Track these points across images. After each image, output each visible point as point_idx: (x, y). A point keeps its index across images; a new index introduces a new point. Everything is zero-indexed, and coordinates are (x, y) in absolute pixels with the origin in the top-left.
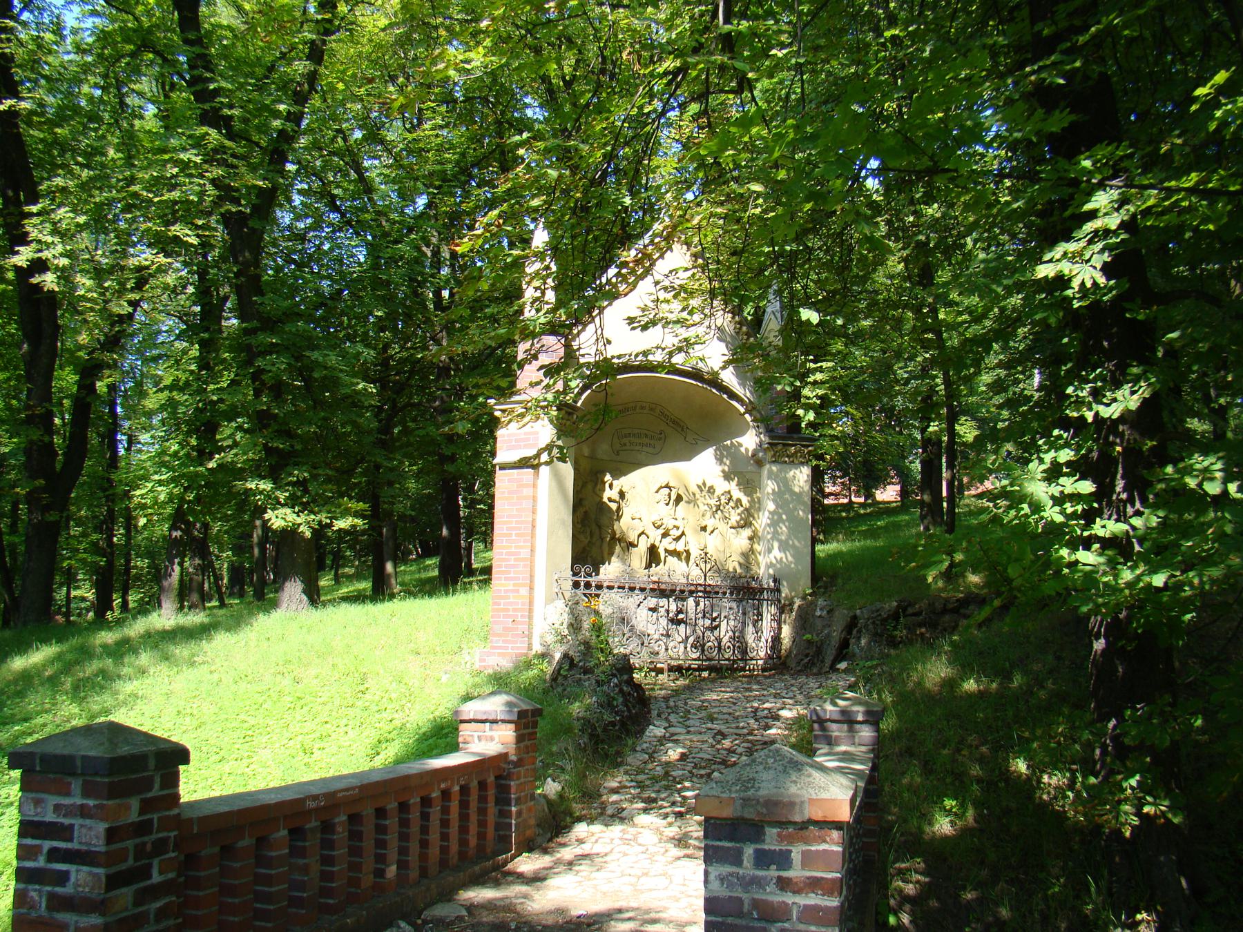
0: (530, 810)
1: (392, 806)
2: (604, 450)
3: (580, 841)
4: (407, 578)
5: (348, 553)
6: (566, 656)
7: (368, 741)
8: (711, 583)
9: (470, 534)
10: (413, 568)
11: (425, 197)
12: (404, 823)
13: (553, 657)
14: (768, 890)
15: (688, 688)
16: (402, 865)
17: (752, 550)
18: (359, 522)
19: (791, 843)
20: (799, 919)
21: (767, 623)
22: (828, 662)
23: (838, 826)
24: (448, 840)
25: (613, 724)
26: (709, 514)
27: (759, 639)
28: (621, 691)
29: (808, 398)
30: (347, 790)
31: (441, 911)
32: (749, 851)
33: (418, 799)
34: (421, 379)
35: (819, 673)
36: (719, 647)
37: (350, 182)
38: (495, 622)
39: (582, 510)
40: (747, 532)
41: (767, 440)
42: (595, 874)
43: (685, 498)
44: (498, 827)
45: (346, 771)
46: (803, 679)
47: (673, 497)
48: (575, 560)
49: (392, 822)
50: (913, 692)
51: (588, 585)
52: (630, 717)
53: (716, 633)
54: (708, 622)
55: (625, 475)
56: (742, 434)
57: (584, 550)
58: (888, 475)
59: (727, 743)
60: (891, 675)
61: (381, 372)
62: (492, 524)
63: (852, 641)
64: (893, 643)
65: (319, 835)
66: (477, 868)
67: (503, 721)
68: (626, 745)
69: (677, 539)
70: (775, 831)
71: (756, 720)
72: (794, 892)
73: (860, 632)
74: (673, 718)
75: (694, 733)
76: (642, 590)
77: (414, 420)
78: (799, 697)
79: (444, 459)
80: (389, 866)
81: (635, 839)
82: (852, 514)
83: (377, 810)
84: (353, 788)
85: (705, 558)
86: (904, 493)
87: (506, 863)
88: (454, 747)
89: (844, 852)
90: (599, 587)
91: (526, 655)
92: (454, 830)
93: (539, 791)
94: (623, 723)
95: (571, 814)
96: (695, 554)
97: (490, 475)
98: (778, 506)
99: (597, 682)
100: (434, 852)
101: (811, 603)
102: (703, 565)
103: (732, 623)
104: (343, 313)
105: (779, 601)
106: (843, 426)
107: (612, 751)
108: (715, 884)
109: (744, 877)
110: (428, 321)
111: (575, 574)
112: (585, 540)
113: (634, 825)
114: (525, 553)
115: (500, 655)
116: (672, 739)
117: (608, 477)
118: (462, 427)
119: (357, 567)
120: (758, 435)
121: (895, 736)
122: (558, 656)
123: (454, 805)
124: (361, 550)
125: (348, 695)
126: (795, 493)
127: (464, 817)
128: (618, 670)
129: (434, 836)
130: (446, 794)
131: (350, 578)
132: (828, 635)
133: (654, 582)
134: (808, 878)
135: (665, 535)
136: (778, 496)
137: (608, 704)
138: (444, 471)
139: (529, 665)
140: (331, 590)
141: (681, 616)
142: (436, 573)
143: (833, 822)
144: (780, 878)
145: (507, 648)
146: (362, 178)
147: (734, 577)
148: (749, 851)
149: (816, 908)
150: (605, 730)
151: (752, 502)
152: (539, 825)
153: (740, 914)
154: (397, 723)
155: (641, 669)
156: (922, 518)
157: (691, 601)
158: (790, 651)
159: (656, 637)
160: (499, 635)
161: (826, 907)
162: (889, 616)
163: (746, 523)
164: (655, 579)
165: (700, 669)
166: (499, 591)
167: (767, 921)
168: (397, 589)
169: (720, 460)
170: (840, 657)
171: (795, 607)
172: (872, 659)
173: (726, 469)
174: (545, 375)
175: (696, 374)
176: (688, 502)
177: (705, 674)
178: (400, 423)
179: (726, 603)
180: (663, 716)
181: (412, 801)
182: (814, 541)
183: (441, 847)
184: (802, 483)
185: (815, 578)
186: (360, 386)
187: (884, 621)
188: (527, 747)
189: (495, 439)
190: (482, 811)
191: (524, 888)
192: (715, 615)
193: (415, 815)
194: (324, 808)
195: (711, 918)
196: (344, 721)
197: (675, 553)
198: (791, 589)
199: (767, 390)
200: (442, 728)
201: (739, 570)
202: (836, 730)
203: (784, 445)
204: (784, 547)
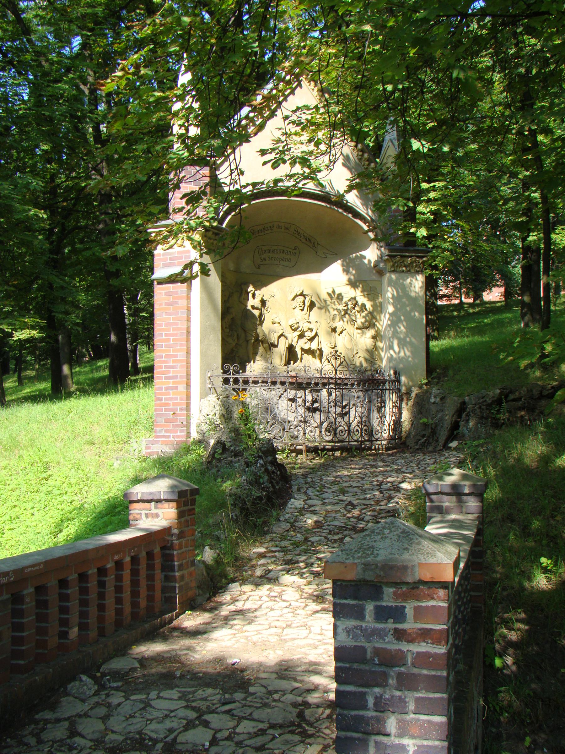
0: (191, 574)
1: (73, 577)
2: (247, 265)
3: (234, 600)
4: (82, 378)
5: (29, 358)
6: (219, 442)
7: (52, 520)
8: (341, 376)
9: (135, 338)
10: (86, 369)
11: (79, 38)
12: (84, 591)
13: (208, 443)
14: (387, 640)
15: (323, 466)
16: (83, 627)
17: (375, 346)
18: (35, 333)
19: (405, 600)
20: (413, 664)
21: (389, 408)
23: (444, 585)
24: (122, 604)
25: (260, 498)
26: (338, 318)
27: (383, 423)
28: (267, 470)
29: (423, 214)
30: (33, 566)
31: (117, 664)
32: (370, 607)
33: (96, 570)
34: (86, 205)
35: (434, 451)
36: (349, 431)
37: (9, 23)
38: (157, 415)
39: (229, 317)
40: (372, 332)
41: (387, 253)
42: (247, 627)
43: (317, 305)
44: (164, 590)
45: (33, 549)
46: (420, 456)
47: (307, 304)
48: (223, 359)
49: (73, 591)
50: (513, 467)
51: (236, 381)
52: (274, 492)
53: (346, 418)
54: (339, 410)
55: (265, 285)
56: (365, 248)
57: (232, 351)
58: (493, 279)
59: (356, 512)
60: (494, 452)
61: (50, 199)
62: (153, 329)
63: (462, 423)
64: (497, 425)
65: (10, 606)
66: (147, 626)
67: (166, 500)
68: (271, 516)
69: (312, 339)
70: (391, 590)
71: (381, 492)
72: (409, 642)
73: (468, 415)
74: (310, 492)
75: (329, 504)
76: (283, 383)
77: (82, 242)
78: (417, 472)
79: (109, 275)
80: (71, 628)
81: (280, 596)
82: (462, 313)
83: (60, 581)
84: (39, 564)
85: (336, 355)
86: (508, 294)
87: (171, 620)
88: (125, 524)
89: (449, 607)
90: (246, 382)
91: (186, 442)
92: (126, 595)
93: (199, 558)
94: (269, 499)
95: (226, 577)
96: (327, 351)
97: (150, 286)
100: (110, 614)
101: (427, 391)
102: (333, 362)
103: (359, 410)
104: (11, 147)
105: (399, 390)
106: (457, 236)
107: (260, 521)
108: (343, 636)
109: (366, 629)
110: (89, 153)
111: (225, 372)
112: (232, 343)
113: (280, 584)
114: (182, 355)
115: (163, 442)
116: (308, 510)
117: (251, 288)
118: (121, 251)
119: (37, 371)
120: (379, 248)
121: (498, 505)
122: (212, 442)
123: (126, 574)
124: (40, 355)
125: (33, 482)
127: (135, 583)
128: (263, 452)
129: (110, 601)
130: (119, 565)
131: (32, 379)
132: (441, 419)
133: (293, 377)
134: (420, 629)
135: (301, 336)
136: (396, 300)
137: (256, 482)
138: (111, 285)
139: (187, 450)
140: (15, 390)
141: (316, 405)
142: (107, 373)
143: (440, 582)
144: (396, 630)
146: (19, 20)
147: (361, 371)
148: (370, 607)
149: (427, 655)
150: (254, 504)
152: (199, 587)
153: (364, 661)
154: (77, 504)
155: (283, 451)
156: (523, 316)
157: (324, 392)
158: (409, 433)
159: (295, 423)
161: (436, 654)
162: (493, 402)
163: (369, 324)
164: (293, 374)
165: (333, 449)
166: (161, 388)
167: (387, 666)
168: (73, 388)
169: (346, 271)
170: (452, 437)
171: (413, 395)
172: (479, 438)
173: (352, 277)
174: (187, 203)
175: (325, 197)
176: (320, 308)
177: (338, 454)
178: (69, 244)
179: (354, 393)
180: (303, 491)
181: (90, 572)
182: (429, 338)
183: (116, 609)
184: (417, 289)
185: (430, 371)
186: (32, 213)
187: (490, 405)
188: (187, 521)
189: (153, 256)
190: (151, 578)
191: (187, 642)
192: (344, 404)
193: (93, 584)
194: (14, 582)
195: (340, 664)
196: (31, 505)
198: (410, 377)
199: (384, 211)
200: (115, 507)
201: (364, 365)
202: (448, 502)
203: (402, 257)
204: (402, 344)
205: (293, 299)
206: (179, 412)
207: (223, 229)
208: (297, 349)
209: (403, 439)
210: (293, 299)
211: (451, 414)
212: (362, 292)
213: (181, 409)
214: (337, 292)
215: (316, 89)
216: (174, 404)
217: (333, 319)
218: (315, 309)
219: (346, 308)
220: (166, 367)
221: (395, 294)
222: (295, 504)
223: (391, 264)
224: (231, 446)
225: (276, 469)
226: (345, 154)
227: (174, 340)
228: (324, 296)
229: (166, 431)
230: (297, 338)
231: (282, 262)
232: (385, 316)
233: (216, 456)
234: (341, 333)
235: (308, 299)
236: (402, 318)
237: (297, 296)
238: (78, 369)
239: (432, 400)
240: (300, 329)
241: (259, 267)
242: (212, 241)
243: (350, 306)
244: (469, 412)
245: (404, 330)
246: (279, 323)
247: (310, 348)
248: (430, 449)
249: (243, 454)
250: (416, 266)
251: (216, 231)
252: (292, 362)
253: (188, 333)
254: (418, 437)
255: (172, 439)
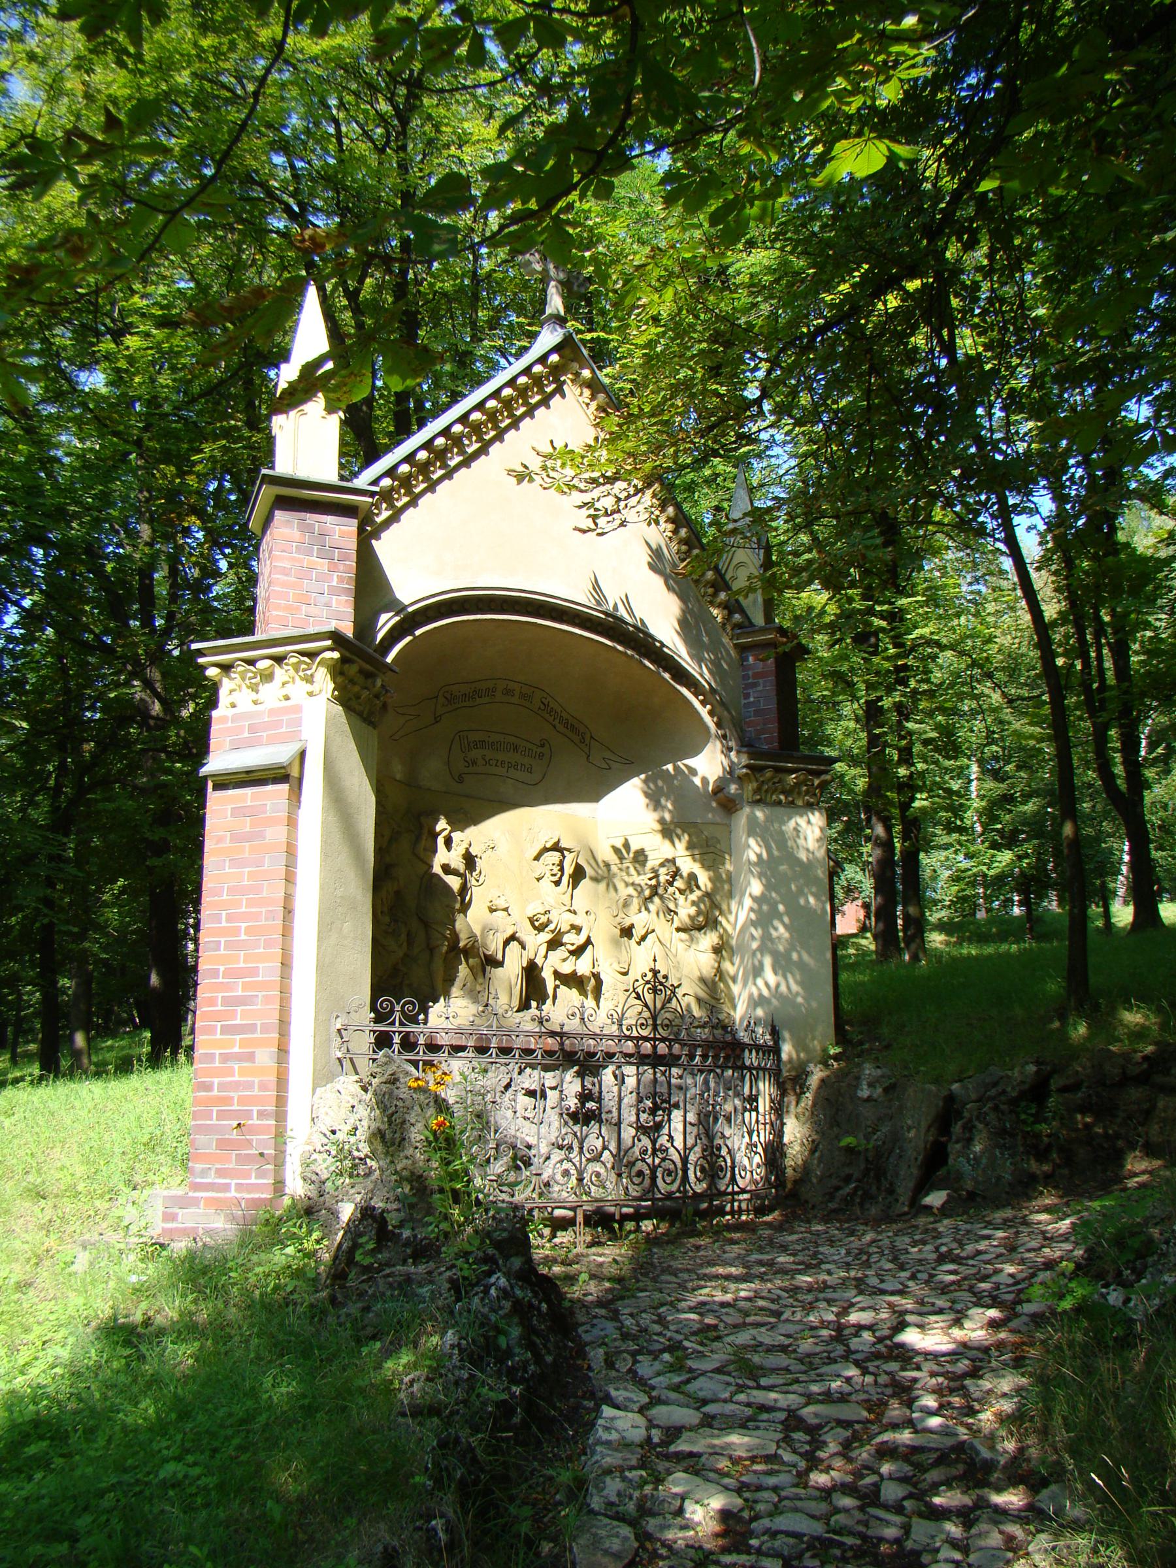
2: (433, 771)
6: (366, 1213)
13: (335, 1214)
17: (719, 971)
22: (904, 1189)
25: (505, 1408)
26: (636, 903)
35: (887, 1218)
38: (200, 1129)
40: (709, 939)
41: (744, 760)
47: (569, 869)
48: (377, 990)
51: (408, 1044)
55: (476, 822)
56: (695, 751)
63: (955, 1148)
69: (578, 952)
73: (969, 1128)
90: (433, 1048)
98: (768, 887)
99: (454, 1284)
102: (649, 998)
114: (269, 970)
115: (210, 1202)
117: (442, 825)
122: (347, 1211)
126: (798, 861)
128: (497, 1245)
135: (554, 944)
136: (767, 868)
145: (226, 1188)
151: (715, 880)
158: (805, 1170)
159: (544, 1149)
160: (206, 1158)
162: (1022, 1095)
163: (705, 921)
169: (654, 799)
176: (596, 880)
187: (1014, 1102)
197: (573, 980)
198: (799, 1045)
203: (778, 770)
204: (782, 965)
205: (537, 858)
206: (255, 1121)
207: (386, 665)
208: (543, 974)
209: (789, 1186)
210: (537, 858)
211: (924, 1125)
212: (688, 849)
213: (261, 1114)
214: (634, 847)
215: (594, 405)
216: (241, 1101)
217: (626, 904)
218: (585, 883)
219: (653, 882)
220: (227, 1001)
221: (765, 855)
222: (619, 1424)
223: (755, 785)
224: (401, 1225)
225: (536, 1294)
226: (654, 547)
227: (249, 931)
228: (605, 854)
229: (220, 1173)
230: (544, 948)
231: (511, 770)
232: (740, 903)
233: (358, 1257)
234: (643, 938)
235: (569, 857)
236: (781, 908)
237: (546, 850)
238: (109, 1043)
239: (864, 1092)
240: (552, 927)
241: (460, 780)
242: (356, 689)
243: (662, 879)
244: (970, 1120)
245: (787, 935)
246: (506, 910)
247: (574, 973)
248: (874, 1211)
249: (439, 1252)
250: (807, 792)
251: (368, 667)
252: (534, 1004)
253: (288, 911)
254: (834, 1182)
255: (233, 1193)
